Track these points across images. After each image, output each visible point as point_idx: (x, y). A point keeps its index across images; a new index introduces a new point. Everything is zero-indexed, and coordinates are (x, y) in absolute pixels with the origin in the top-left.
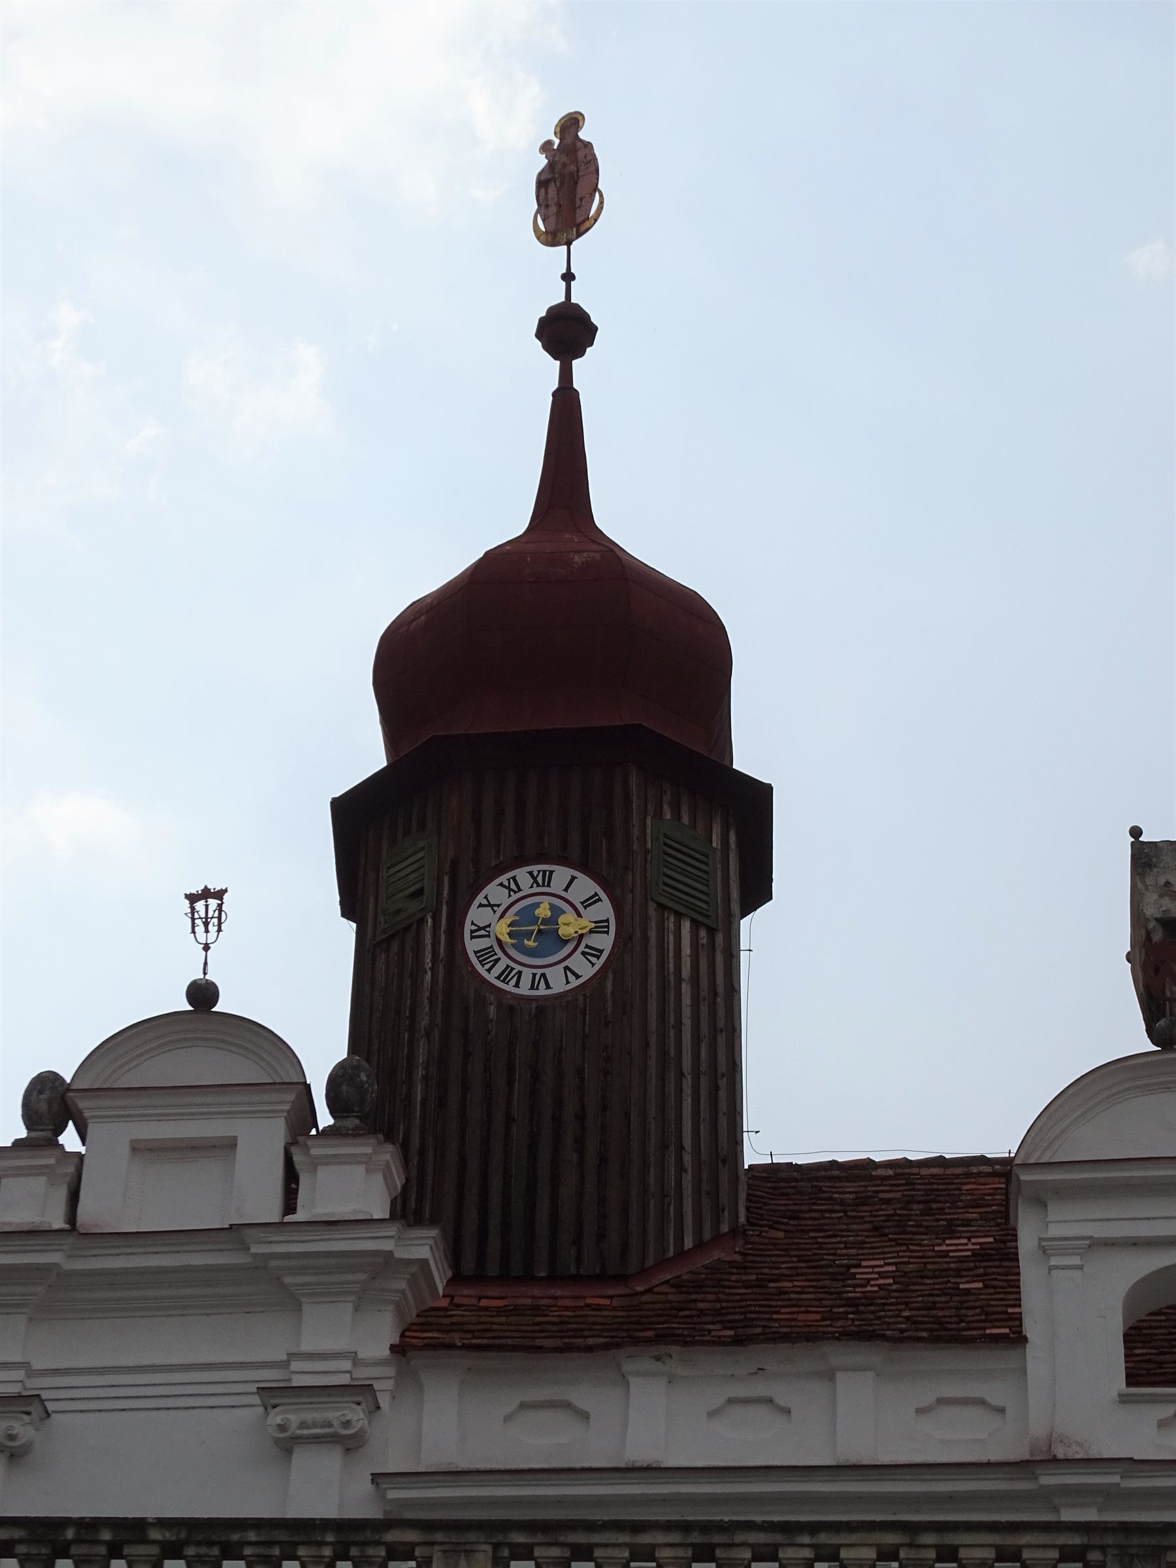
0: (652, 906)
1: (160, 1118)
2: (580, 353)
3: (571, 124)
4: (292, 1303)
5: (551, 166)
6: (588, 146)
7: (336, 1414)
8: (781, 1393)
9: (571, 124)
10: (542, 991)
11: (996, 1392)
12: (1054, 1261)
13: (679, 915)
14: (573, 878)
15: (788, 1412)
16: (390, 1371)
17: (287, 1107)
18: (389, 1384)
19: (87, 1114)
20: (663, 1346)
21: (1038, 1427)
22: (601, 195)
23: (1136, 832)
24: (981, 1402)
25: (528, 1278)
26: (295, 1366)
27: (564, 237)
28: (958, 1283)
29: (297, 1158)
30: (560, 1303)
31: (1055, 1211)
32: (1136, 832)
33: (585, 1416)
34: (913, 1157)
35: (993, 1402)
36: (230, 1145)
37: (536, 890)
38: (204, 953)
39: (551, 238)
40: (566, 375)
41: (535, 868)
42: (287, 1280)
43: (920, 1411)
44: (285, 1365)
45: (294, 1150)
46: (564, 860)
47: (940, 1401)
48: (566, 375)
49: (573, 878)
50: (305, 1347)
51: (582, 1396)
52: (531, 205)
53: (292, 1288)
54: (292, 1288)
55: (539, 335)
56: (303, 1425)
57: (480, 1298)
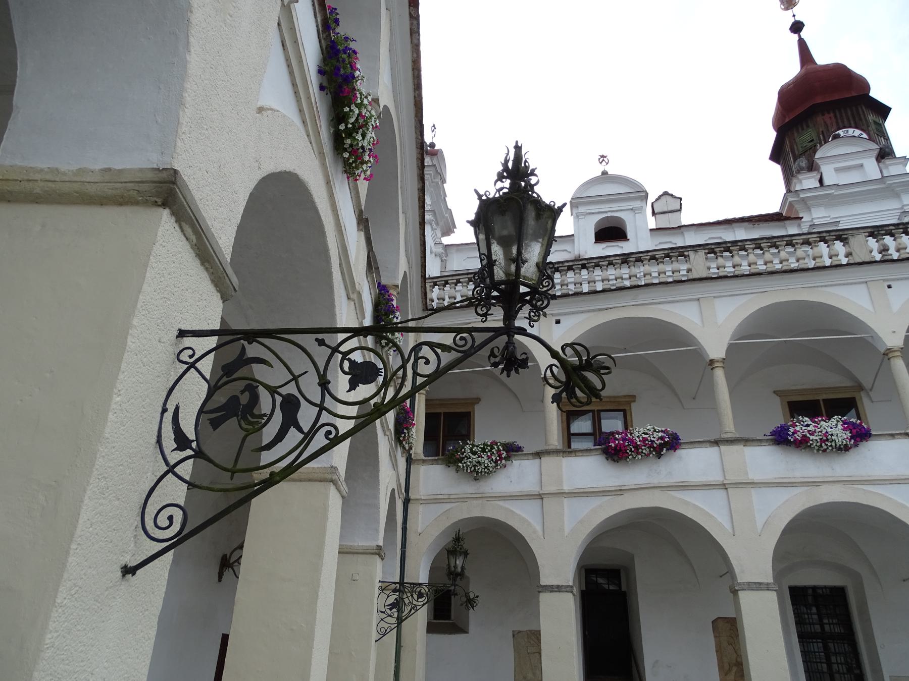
0: (876, 135)
1: (840, 162)
2: (801, 31)
13: (881, 136)
14: (854, 131)
19: (819, 164)
20: (502, 253)
21: (576, 253)
27: (791, 8)
28: (792, 240)
33: (622, 247)
35: (569, 250)
36: (862, 166)
37: (845, 134)
39: (787, 9)
40: (800, 36)
41: (844, 130)
46: (850, 127)
48: (800, 36)
49: (854, 131)
53: (897, 189)
54: (897, 189)
55: (792, 32)
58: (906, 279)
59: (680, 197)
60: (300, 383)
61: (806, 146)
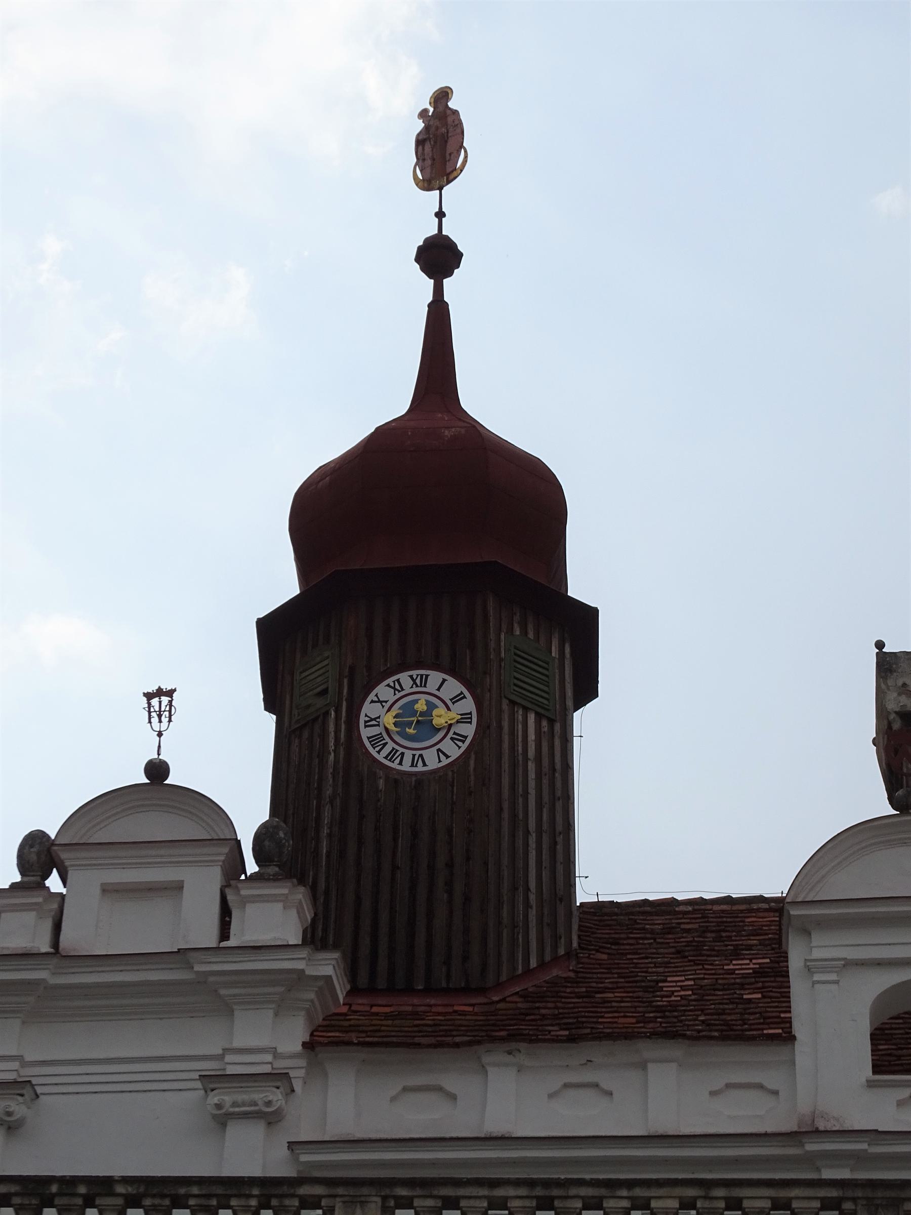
0: (505, 702)
1: (124, 866)
2: (450, 274)
3: (442, 96)
4: (226, 1010)
5: (427, 128)
6: (456, 113)
7: (260, 1095)
8: (605, 1079)
9: (442, 96)
10: (420, 768)
11: (772, 1079)
12: (816, 977)
13: (526, 709)
14: (444, 681)
15: (610, 1094)
16: (302, 1063)
17: (222, 858)
18: (301, 1073)
19: (67, 863)
22: (466, 151)
23: (880, 645)
24: (760, 1087)
25: (409, 990)
26: (229, 1058)
27: (437, 183)
29: (230, 898)
30: (434, 1009)
31: (817, 938)
32: (880, 645)
33: (453, 1097)
34: (707, 896)
36: (178, 887)
38: (158, 738)
39: (427, 184)
40: (438, 291)
41: (414, 673)
42: (223, 992)
43: (713, 1094)
44: (221, 1057)
45: (228, 891)
46: (437, 667)
47: (728, 1086)
48: (438, 291)
49: (444, 681)
50: (237, 1044)
51: (450, 1082)
52: (412, 159)
53: (226, 998)
54: (226, 998)
55: (417, 260)
56: (235, 1104)
57: (372, 1006)
58: (909, 1144)
59: (436, 752)
60: (438, 207)
61: (309, 706)
